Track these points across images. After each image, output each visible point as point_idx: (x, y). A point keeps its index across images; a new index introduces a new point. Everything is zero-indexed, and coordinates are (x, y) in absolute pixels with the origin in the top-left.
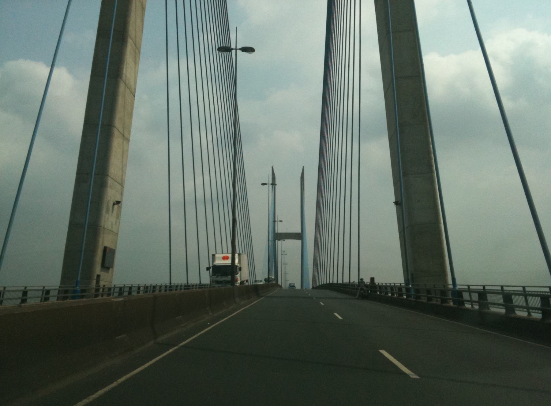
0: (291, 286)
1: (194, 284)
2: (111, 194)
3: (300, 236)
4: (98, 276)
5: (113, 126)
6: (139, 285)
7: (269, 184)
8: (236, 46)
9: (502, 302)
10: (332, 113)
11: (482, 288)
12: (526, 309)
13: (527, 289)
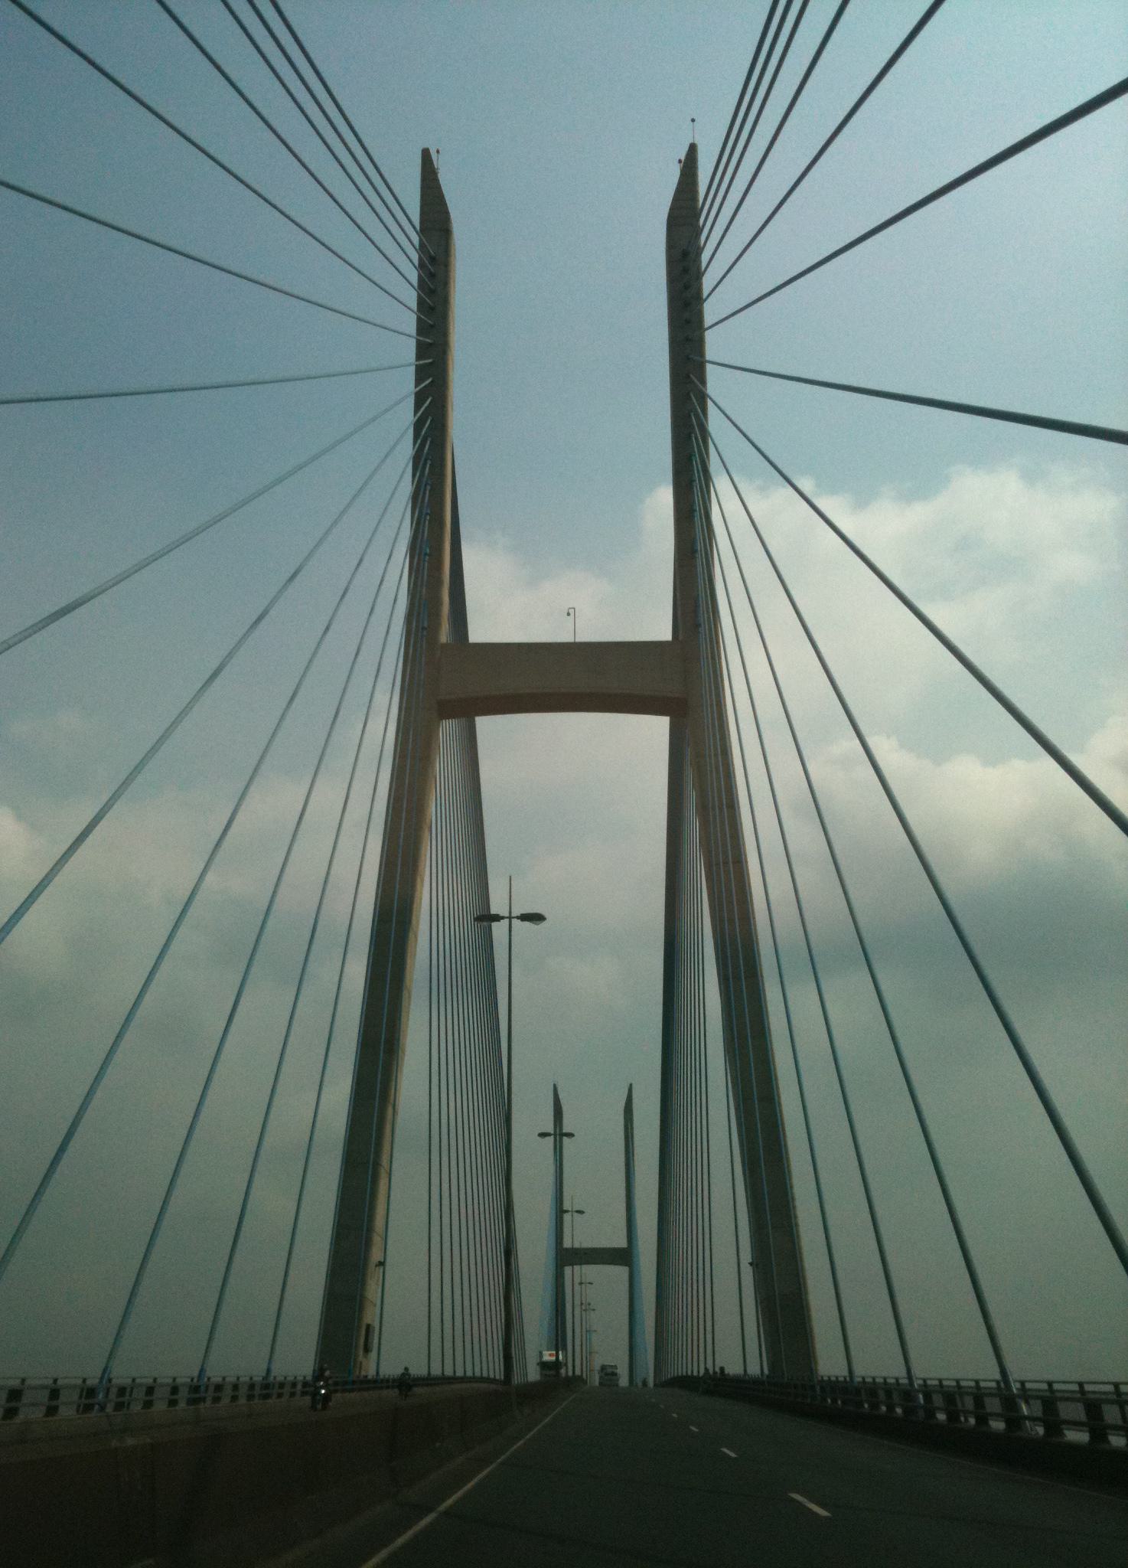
0: (607, 1374)
1: (389, 1376)
2: (376, 1255)
3: (623, 1257)
4: (361, 1363)
5: (381, 1165)
6: (174, 1379)
7: (510, 918)
8: (510, 912)
9: (1082, 1416)
10: (695, 1044)
11: (1045, 1386)
12: (1044, 1422)
13: (1056, 1387)
